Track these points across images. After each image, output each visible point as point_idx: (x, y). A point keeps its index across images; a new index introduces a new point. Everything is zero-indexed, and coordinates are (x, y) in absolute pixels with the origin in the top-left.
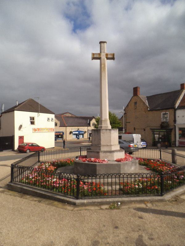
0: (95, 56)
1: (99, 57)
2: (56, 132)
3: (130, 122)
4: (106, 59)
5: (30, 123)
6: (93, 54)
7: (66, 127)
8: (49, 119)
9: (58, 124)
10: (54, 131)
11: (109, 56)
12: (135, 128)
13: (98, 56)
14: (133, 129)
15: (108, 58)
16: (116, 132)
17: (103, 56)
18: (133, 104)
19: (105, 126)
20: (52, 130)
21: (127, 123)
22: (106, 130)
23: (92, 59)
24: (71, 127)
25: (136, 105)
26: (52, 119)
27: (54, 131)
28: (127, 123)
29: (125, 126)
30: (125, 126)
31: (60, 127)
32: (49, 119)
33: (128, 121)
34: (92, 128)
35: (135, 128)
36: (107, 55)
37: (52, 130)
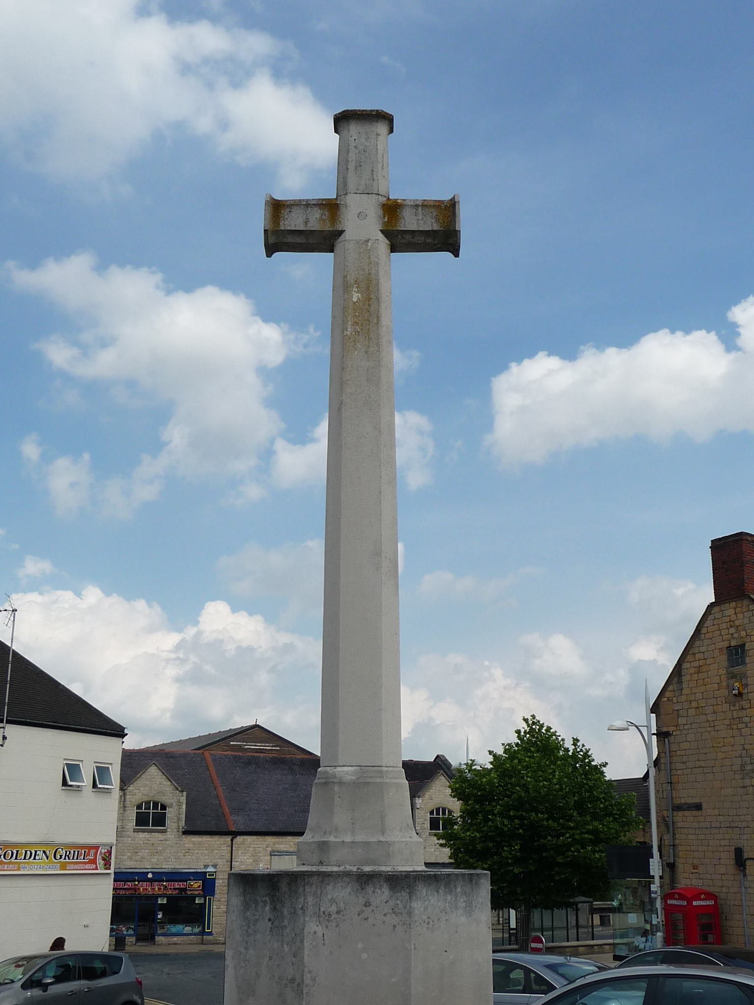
0: (294, 221)
1: (327, 227)
2: (120, 877)
3: (698, 807)
4: (383, 243)
5: (137, 803)
6: (277, 207)
7: (234, 834)
8: (73, 770)
9: (170, 813)
10: (107, 865)
11: (410, 222)
12: (739, 852)
13: (315, 221)
14: (728, 859)
15: (401, 241)
16: (469, 909)
17: (362, 224)
18: (718, 667)
19: (359, 838)
20: (93, 862)
21: (678, 808)
22: (364, 880)
23: (269, 254)
24: (270, 840)
25: (737, 670)
26: (102, 772)
27: (107, 865)
28: (678, 808)
29: (667, 838)
30: (667, 838)
31: (186, 833)
32: (73, 770)
33: (685, 796)
34: (596, 823)
35: (739, 852)
36: (392, 209)
37: (93, 862)
